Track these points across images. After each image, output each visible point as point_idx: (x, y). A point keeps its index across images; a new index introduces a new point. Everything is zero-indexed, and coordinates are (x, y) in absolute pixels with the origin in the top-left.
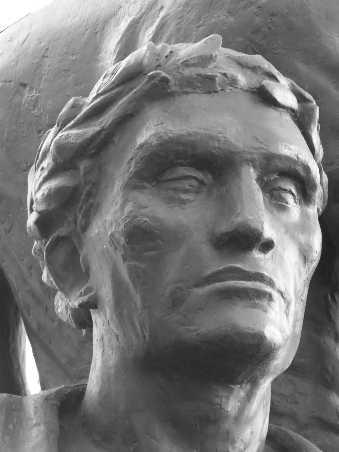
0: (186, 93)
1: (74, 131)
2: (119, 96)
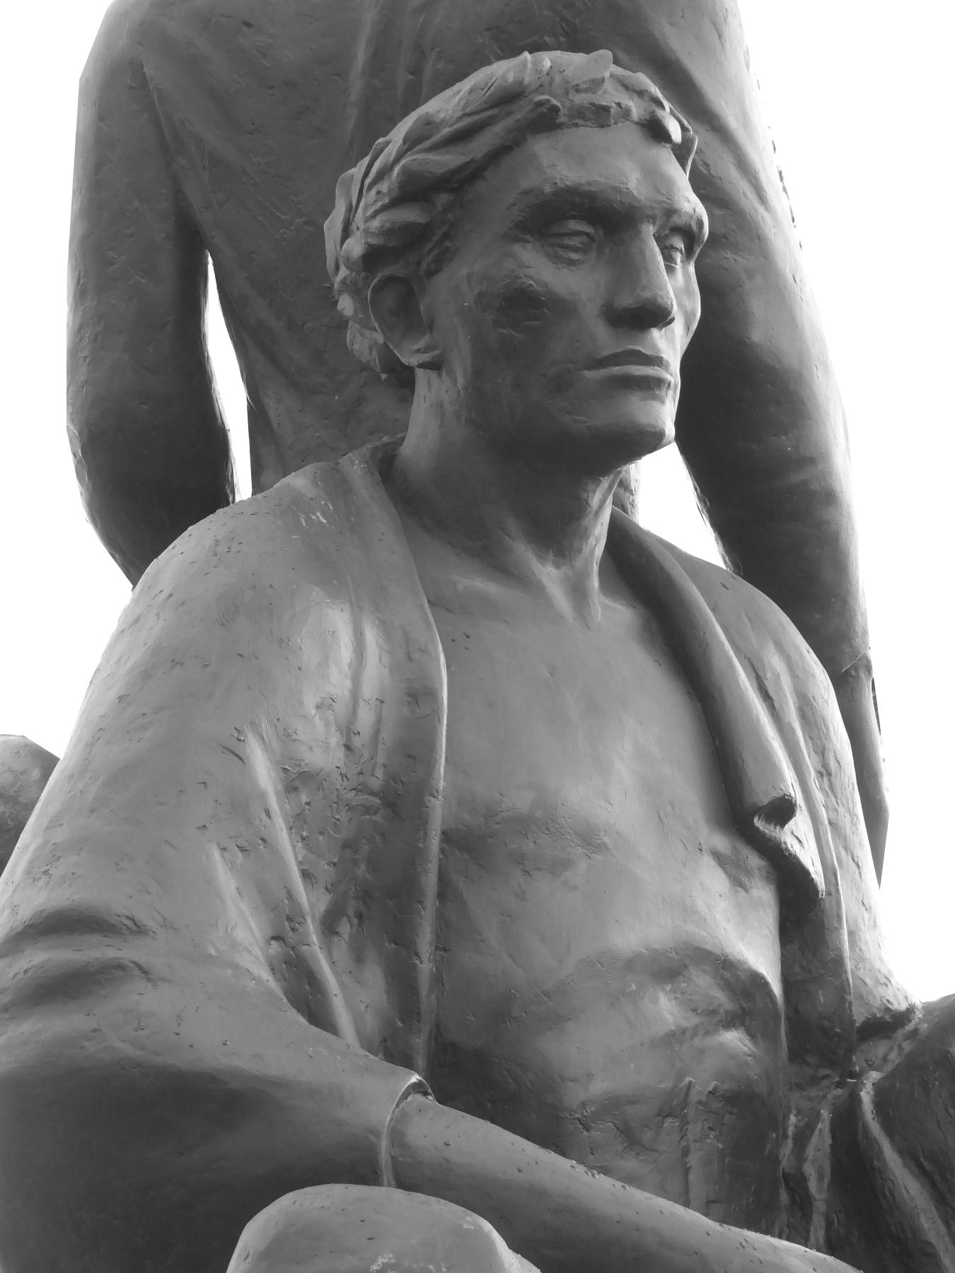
0: (577, 125)
1: (432, 157)
2: (490, 122)
